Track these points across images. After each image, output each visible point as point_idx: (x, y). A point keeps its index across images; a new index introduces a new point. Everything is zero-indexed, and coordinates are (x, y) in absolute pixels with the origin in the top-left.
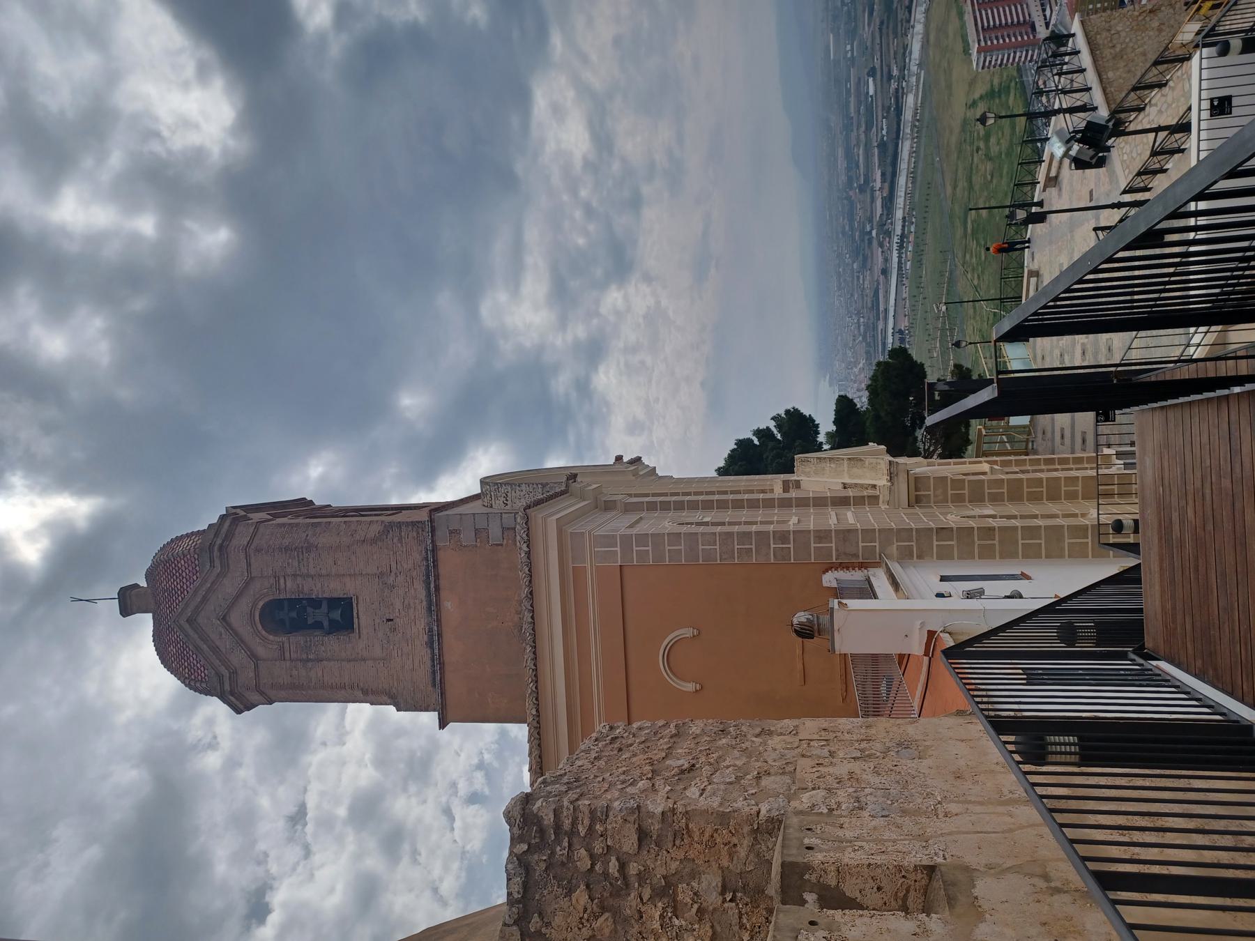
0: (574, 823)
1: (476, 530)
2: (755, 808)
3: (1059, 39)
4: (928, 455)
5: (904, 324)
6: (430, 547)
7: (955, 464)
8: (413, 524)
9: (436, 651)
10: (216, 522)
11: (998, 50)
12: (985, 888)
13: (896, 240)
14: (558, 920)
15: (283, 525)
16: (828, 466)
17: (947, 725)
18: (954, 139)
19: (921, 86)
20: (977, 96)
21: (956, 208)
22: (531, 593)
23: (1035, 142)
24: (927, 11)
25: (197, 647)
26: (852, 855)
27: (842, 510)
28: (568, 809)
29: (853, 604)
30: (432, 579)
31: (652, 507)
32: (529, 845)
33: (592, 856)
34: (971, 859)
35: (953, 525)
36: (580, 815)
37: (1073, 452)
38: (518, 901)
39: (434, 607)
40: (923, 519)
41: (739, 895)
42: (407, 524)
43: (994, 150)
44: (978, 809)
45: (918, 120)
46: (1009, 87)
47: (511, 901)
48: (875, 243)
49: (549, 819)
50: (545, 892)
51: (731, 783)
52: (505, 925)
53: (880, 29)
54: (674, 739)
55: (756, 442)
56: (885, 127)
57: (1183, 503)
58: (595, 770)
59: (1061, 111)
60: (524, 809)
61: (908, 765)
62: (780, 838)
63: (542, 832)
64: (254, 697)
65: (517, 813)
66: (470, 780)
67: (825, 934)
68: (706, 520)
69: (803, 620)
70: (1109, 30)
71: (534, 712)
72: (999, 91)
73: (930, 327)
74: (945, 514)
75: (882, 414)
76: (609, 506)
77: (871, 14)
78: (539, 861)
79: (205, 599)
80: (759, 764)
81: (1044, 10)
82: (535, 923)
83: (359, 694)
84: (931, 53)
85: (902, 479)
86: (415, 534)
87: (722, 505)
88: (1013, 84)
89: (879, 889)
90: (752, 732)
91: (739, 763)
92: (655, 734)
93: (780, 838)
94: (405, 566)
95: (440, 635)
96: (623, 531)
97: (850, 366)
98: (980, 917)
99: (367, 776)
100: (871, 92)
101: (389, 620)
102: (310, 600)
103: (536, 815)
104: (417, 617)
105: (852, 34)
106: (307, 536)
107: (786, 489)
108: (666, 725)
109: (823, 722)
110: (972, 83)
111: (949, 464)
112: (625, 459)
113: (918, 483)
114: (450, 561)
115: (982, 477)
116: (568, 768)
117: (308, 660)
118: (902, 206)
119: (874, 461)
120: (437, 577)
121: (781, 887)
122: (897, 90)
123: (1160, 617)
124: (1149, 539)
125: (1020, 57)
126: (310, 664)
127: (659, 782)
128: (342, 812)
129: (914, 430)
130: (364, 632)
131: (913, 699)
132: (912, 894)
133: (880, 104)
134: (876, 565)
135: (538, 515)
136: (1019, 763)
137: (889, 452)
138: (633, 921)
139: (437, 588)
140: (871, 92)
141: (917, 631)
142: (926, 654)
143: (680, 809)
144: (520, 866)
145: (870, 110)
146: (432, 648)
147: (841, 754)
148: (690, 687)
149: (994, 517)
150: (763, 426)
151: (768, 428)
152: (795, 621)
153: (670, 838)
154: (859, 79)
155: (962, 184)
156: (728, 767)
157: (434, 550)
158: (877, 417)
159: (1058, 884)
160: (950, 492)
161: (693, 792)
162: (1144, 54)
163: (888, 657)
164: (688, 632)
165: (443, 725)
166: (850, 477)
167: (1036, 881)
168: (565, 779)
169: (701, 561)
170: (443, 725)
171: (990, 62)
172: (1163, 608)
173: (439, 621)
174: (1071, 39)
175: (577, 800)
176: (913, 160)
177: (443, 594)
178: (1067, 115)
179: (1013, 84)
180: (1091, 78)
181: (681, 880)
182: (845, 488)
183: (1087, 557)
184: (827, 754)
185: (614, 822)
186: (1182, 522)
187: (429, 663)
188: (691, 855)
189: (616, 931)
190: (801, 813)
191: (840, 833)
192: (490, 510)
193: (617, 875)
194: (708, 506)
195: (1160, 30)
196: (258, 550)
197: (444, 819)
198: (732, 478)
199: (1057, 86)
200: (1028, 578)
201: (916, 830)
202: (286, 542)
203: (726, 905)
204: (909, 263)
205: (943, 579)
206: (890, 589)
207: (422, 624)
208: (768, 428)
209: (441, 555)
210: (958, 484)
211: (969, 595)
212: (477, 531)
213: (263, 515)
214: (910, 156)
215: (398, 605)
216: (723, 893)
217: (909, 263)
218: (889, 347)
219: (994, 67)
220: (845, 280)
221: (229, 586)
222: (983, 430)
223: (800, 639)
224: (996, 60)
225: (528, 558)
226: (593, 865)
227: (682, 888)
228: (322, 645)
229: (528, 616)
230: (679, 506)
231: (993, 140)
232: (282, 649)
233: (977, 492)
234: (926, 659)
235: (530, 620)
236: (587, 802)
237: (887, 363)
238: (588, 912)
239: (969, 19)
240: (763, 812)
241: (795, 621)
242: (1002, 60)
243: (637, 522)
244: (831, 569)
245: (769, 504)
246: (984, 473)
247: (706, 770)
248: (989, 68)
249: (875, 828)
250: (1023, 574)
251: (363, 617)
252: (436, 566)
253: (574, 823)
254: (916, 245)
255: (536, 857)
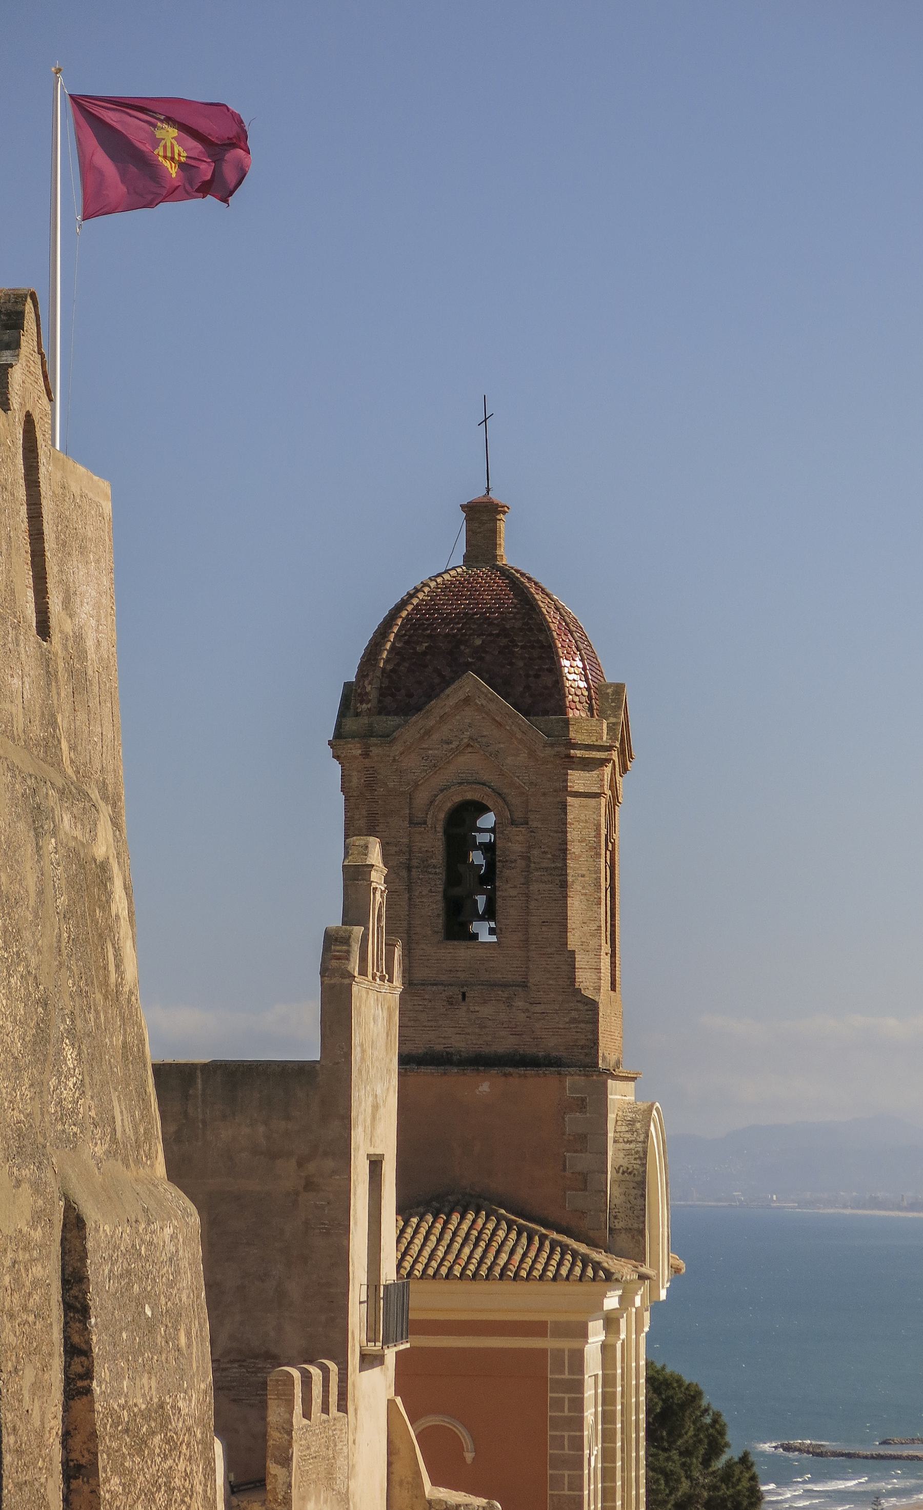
104: (468, 1037)
106: (583, 876)
151: (727, 1445)
169: (551, 1452)
208: (727, 1445)
228: (430, 891)
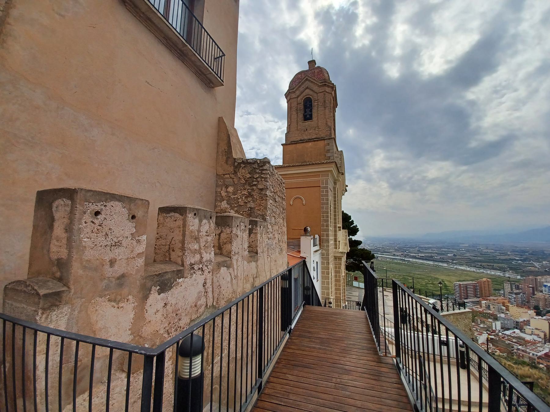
0: (264, 174)
1: (329, 150)
2: (268, 215)
3: (463, 305)
4: (346, 262)
5: (379, 259)
6: (325, 138)
7: (344, 268)
8: (331, 134)
9: (299, 142)
10: (332, 82)
11: (459, 289)
12: (253, 264)
13: (403, 258)
14: (243, 171)
15: (331, 100)
16: (344, 238)
17: (286, 260)
18: (432, 275)
19: (449, 268)
20: (446, 282)
21: (412, 274)
22: (314, 164)
23: (433, 296)
24: (474, 272)
25: (300, 82)
26: (259, 236)
27: (333, 240)
28: (267, 172)
29: (312, 241)
30: (317, 139)
31: (335, 194)
32: (259, 163)
33: (257, 178)
34: (259, 262)
35: (330, 266)
36: (265, 175)
37: (347, 295)
38: (247, 161)
39: (309, 140)
40: (331, 259)
41: (250, 211)
42: (331, 132)
43: (429, 285)
44: (269, 265)
45: (439, 267)
46: (448, 291)
47: (247, 160)
48: (403, 253)
49: (265, 168)
50: (249, 168)
51: (273, 210)
52: (242, 159)
53: (469, 258)
54: (282, 198)
55: (350, 221)
56: (437, 258)
57: (342, 319)
58: (275, 179)
59: (442, 303)
60: (267, 162)
61: (278, 250)
62: (262, 221)
63: (262, 166)
64: (288, 98)
65: (266, 160)
66: (260, 153)
67: (244, 229)
68: (331, 207)
69: (308, 229)
70: (465, 318)
71: (285, 166)
72: (446, 288)
73: (378, 265)
74: (332, 264)
75: (357, 252)
76: (335, 183)
77: (474, 256)
78: (256, 166)
79: (312, 82)
80: (277, 217)
81: (471, 302)
82: (243, 165)
83: (289, 124)
84: (460, 271)
85: (341, 255)
86: (328, 134)
87: (335, 212)
88: (448, 292)
89: (253, 242)
90: (284, 216)
91: (277, 212)
92: (283, 193)
93: (262, 221)
94: (320, 132)
95: (303, 142)
96: (329, 187)
97: (369, 245)
98: (248, 263)
99: (259, 128)
100: (448, 255)
101: (307, 130)
102: (312, 109)
103: (265, 165)
105: (468, 251)
107: (339, 227)
108: (285, 196)
109: (286, 232)
110: (450, 281)
111: (344, 266)
112: (347, 188)
113: (340, 258)
114: (321, 144)
115: (341, 273)
116: (275, 172)
117: (297, 111)
118: (413, 260)
119: (346, 249)
120: (317, 141)
121: (252, 220)
122: (449, 262)
123: (313, 309)
124: (326, 309)
125: (457, 295)
126: (296, 111)
127: (273, 193)
128: (250, 124)
129: (352, 259)
130: (304, 123)
131: (291, 253)
132: (252, 249)
133: (445, 257)
134: (320, 247)
135: (333, 165)
136: (281, 275)
137: (347, 252)
138: (244, 188)
139: (315, 141)
140: (448, 255)
141: (306, 255)
142: (301, 257)
143: (268, 198)
144: (254, 162)
145: (443, 254)
146: (300, 141)
147: (279, 236)
148: (291, 203)
149: (331, 275)
150: (354, 222)
152: (308, 227)
153: (261, 196)
154: (453, 252)
155: (419, 276)
156: (276, 210)
157: (324, 140)
158: (356, 250)
159: (255, 280)
160: (337, 266)
161: (271, 201)
162: (457, 326)
163: (300, 248)
164: (304, 203)
165: (282, 145)
166: (342, 243)
167: (255, 275)
168: (273, 172)
170: (282, 145)
171: (456, 287)
172: (316, 311)
173: (307, 142)
174: (463, 308)
175: (269, 174)
176: (427, 264)
177: (313, 142)
178: (440, 305)
179: (448, 292)
180: (451, 312)
181: (252, 198)
182: (339, 241)
183: (322, 295)
184: (279, 233)
185: (264, 183)
186: (337, 318)
187: (296, 140)
188: (258, 201)
189: (242, 184)
190: (267, 226)
191: (264, 234)
192: (334, 153)
193: (253, 184)
194: (335, 208)
195: (464, 331)
196: (325, 94)
197: (251, 147)
198: (341, 214)
199: (449, 303)
200: (317, 281)
201: (264, 251)
202: (327, 101)
203: (247, 208)
204: (396, 261)
205: (317, 262)
206: (315, 250)
207: (306, 138)
209: (323, 142)
210: (340, 268)
211: (314, 268)
212: (329, 150)
213: (333, 95)
214: (428, 264)
215: (310, 132)
216: (250, 208)
217: (396, 261)
218: (375, 255)
219: (454, 288)
220: (392, 245)
221: (315, 88)
222: (352, 275)
223: (303, 229)
224: (456, 288)
225: (323, 163)
226: (255, 178)
227: (251, 199)
229: (308, 163)
230: (335, 201)
231: (432, 285)
232: (300, 104)
233: (337, 272)
234: (299, 257)
235: (307, 164)
236: (268, 177)
237: (371, 253)
238: (246, 178)
239: (471, 282)
240: (267, 217)
241: (308, 227)
242: (456, 290)
243: (331, 190)
244: (319, 237)
245: (335, 223)
246: (342, 274)
247: (275, 205)
248: (454, 286)
249: (265, 242)
250: (318, 280)
251: (308, 123)
252: (320, 140)
253: (264, 174)
254: (401, 263)
255: (257, 165)
